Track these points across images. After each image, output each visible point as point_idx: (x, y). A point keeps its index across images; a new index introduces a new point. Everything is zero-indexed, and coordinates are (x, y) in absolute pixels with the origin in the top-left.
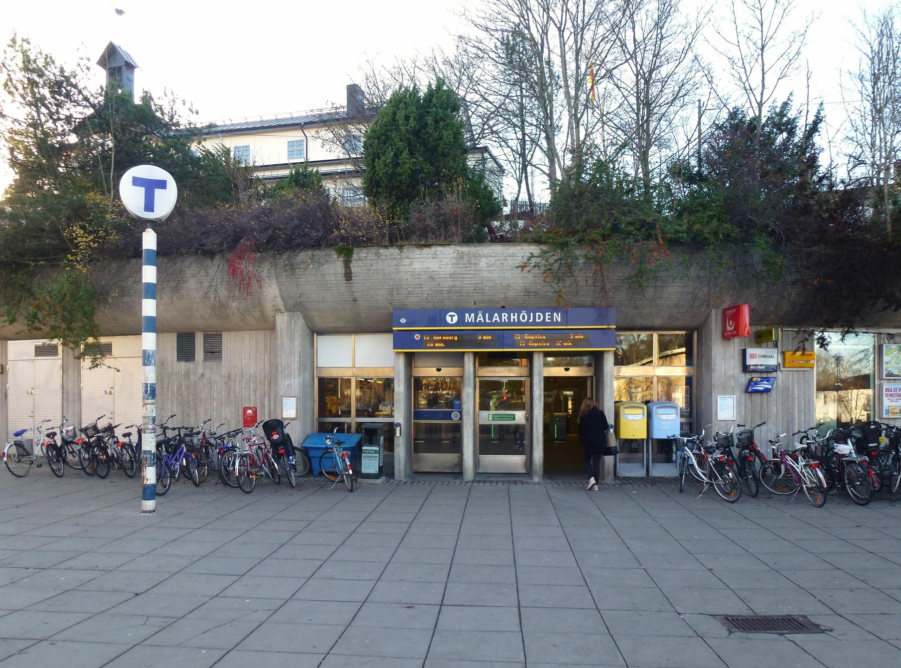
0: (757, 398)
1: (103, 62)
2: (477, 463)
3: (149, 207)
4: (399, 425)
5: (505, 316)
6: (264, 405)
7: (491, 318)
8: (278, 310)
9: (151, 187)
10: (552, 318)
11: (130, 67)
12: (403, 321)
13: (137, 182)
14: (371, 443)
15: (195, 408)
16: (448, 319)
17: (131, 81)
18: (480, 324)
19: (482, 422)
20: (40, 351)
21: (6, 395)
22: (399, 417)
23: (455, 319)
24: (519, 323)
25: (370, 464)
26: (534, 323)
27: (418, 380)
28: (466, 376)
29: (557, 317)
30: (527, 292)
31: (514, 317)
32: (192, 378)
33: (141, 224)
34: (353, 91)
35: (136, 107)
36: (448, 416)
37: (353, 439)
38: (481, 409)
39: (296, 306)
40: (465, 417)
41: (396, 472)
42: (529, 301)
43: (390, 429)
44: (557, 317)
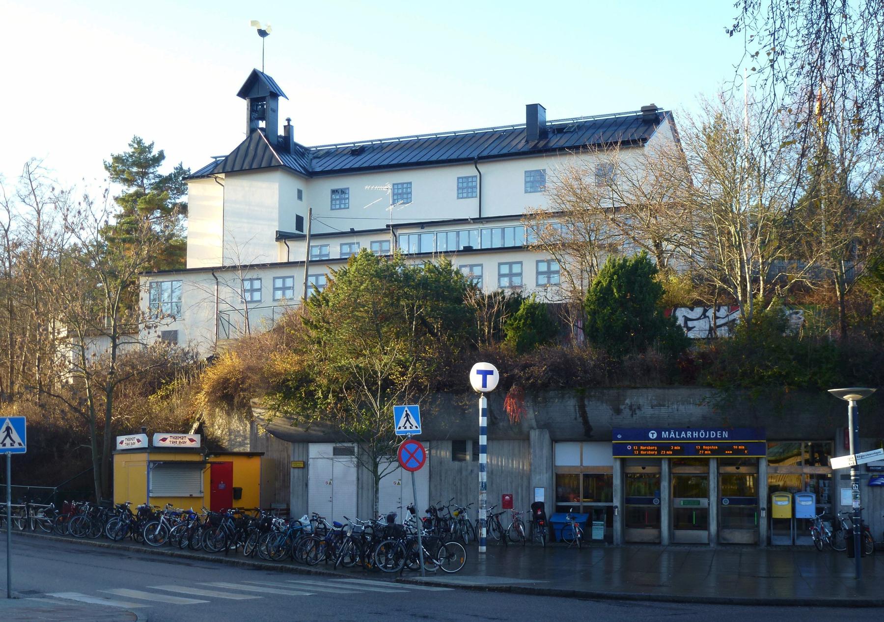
0: (878, 490)
1: (244, 93)
2: (671, 535)
3: (484, 385)
4: (616, 507)
5: (689, 434)
6: (517, 493)
7: (679, 435)
8: (532, 428)
9: (485, 374)
10: (722, 435)
11: (275, 94)
12: (619, 436)
13: (479, 372)
14: (598, 519)
15: (466, 495)
16: (650, 435)
17: (275, 111)
18: (672, 439)
19: (675, 506)
20: (337, 452)
21: (307, 485)
22: (617, 502)
23: (655, 436)
24: (699, 438)
25: (598, 533)
26: (710, 438)
27: (627, 474)
28: (663, 473)
29: (726, 434)
30: (704, 418)
31: (696, 434)
32: (464, 473)
33: (478, 395)
34: (533, 110)
35: (281, 136)
36: (650, 501)
37: (584, 518)
38: (675, 497)
39: (544, 426)
40: (662, 502)
41: (615, 538)
42: (705, 424)
43: (610, 510)
44: (726, 434)
